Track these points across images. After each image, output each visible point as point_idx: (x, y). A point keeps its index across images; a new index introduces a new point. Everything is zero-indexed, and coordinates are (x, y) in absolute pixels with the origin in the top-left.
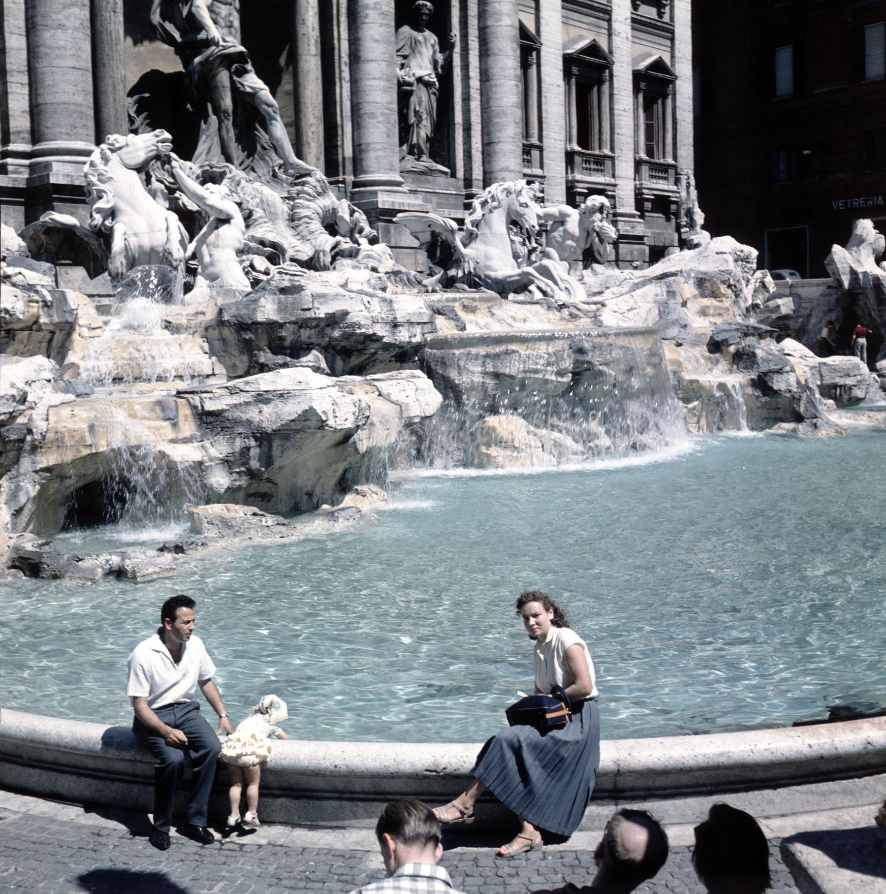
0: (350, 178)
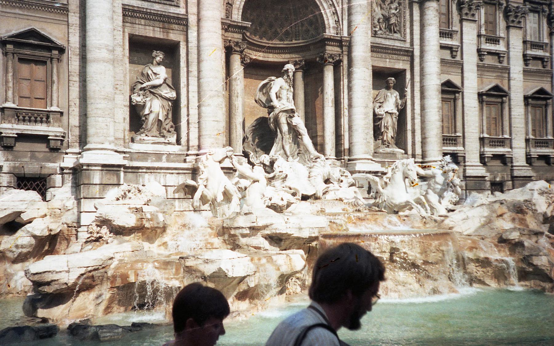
0: (346, 158)
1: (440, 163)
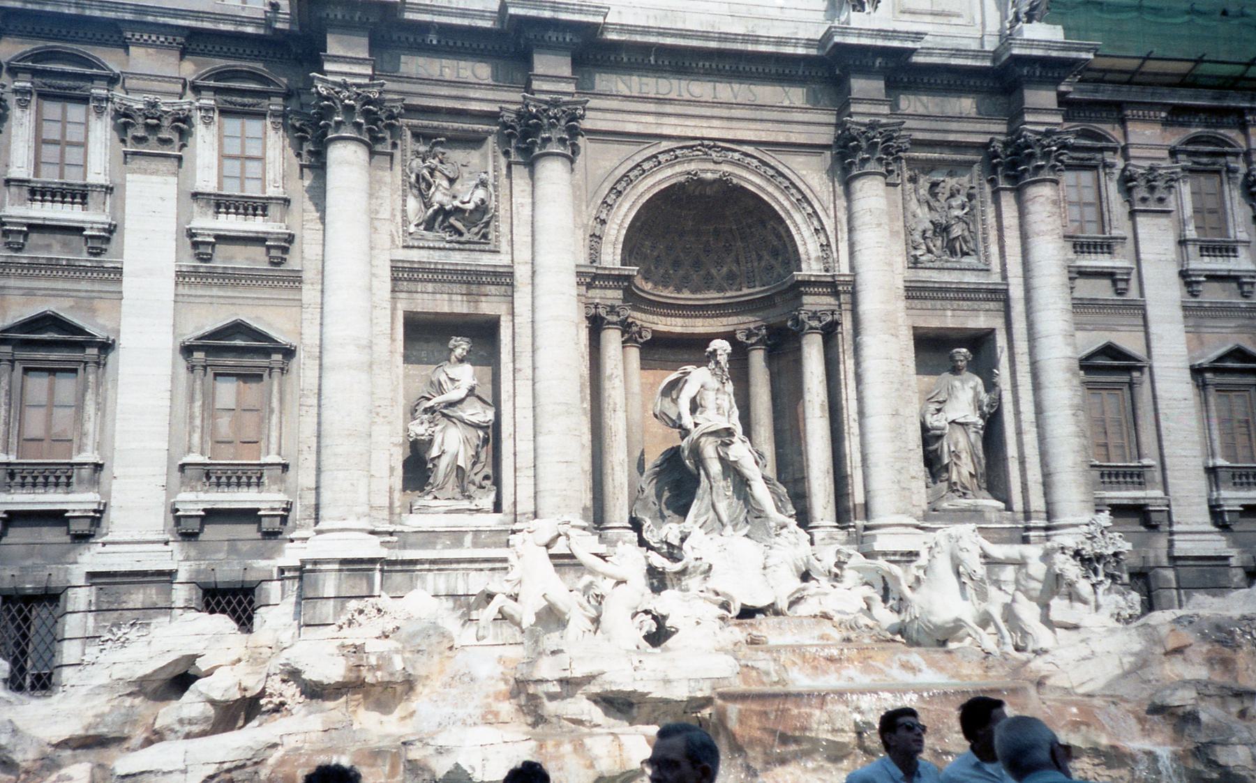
1: (1085, 529)
